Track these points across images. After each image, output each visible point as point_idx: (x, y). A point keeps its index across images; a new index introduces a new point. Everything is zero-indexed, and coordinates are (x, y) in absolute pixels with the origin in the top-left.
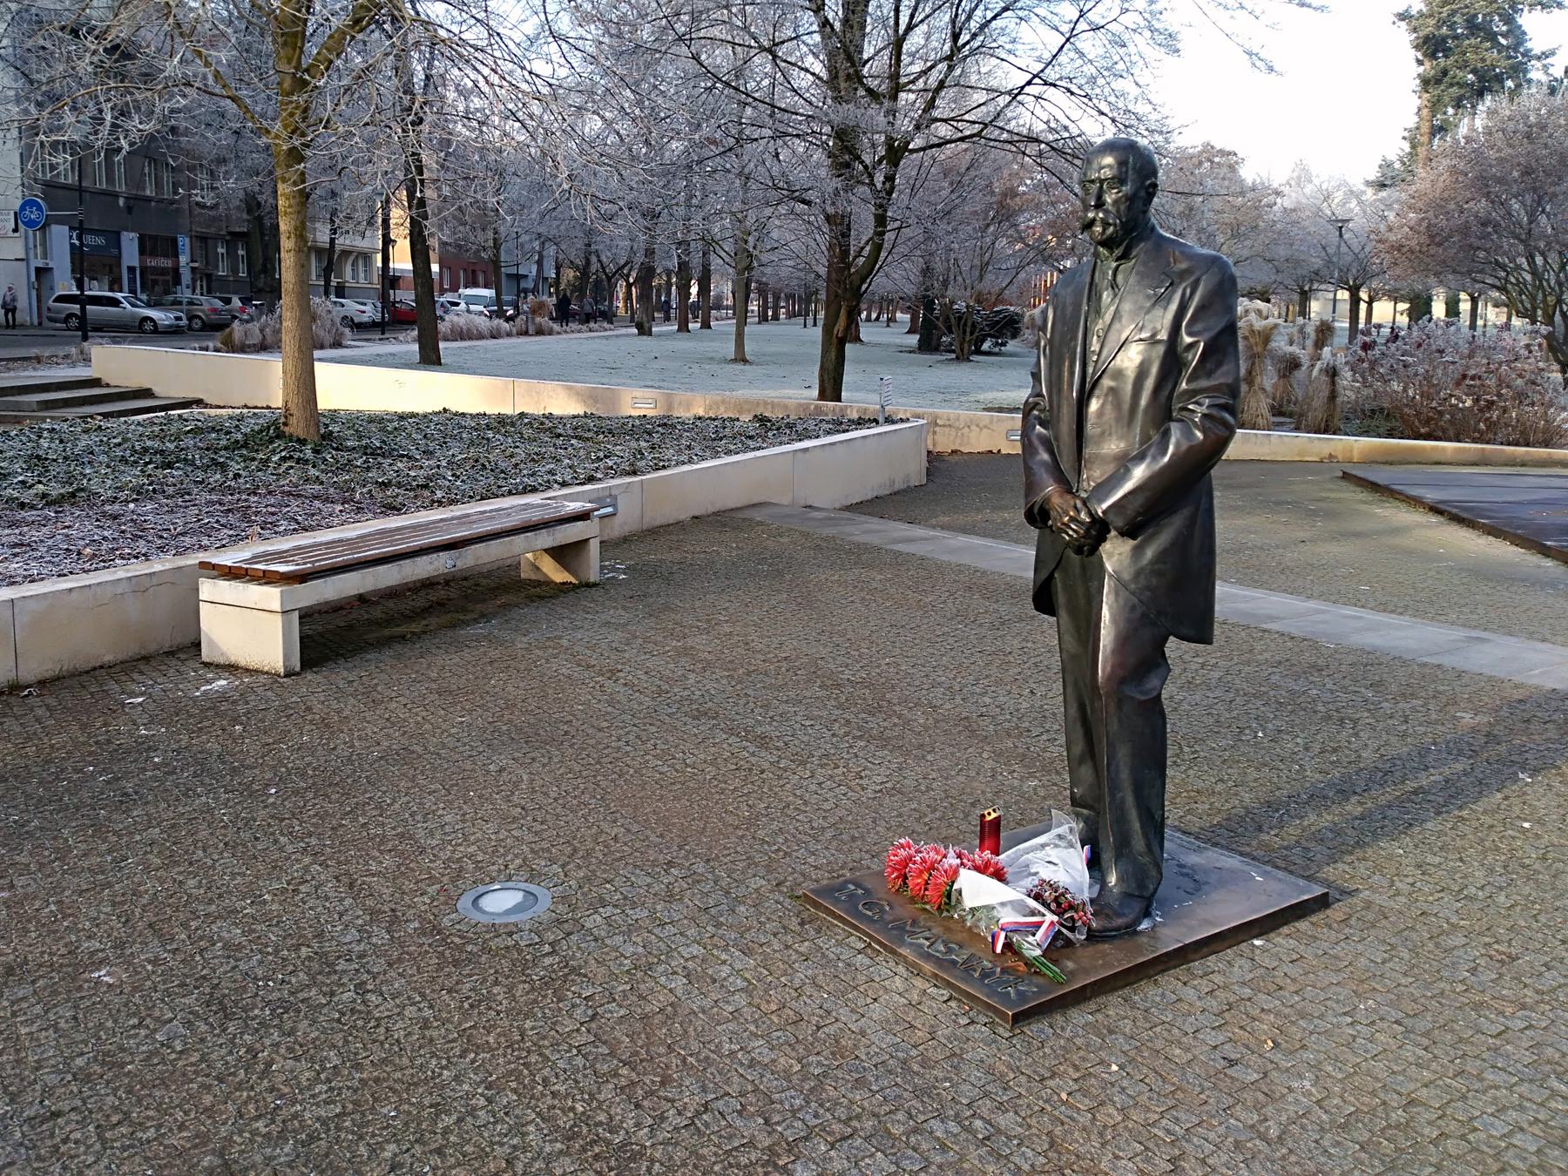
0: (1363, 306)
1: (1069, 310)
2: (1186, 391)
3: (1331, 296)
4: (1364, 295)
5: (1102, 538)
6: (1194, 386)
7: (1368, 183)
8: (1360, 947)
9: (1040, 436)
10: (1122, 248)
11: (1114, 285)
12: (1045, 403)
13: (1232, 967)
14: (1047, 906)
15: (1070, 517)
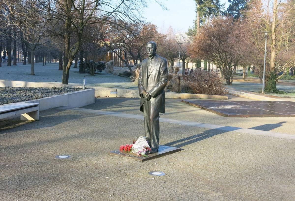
0: (186, 64)
1: (145, 65)
3: (178, 61)
4: (186, 61)
5: (150, 98)
6: (162, 76)
7: (186, 33)
10: (152, 57)
11: (151, 62)
12: (141, 79)
15: (146, 96)
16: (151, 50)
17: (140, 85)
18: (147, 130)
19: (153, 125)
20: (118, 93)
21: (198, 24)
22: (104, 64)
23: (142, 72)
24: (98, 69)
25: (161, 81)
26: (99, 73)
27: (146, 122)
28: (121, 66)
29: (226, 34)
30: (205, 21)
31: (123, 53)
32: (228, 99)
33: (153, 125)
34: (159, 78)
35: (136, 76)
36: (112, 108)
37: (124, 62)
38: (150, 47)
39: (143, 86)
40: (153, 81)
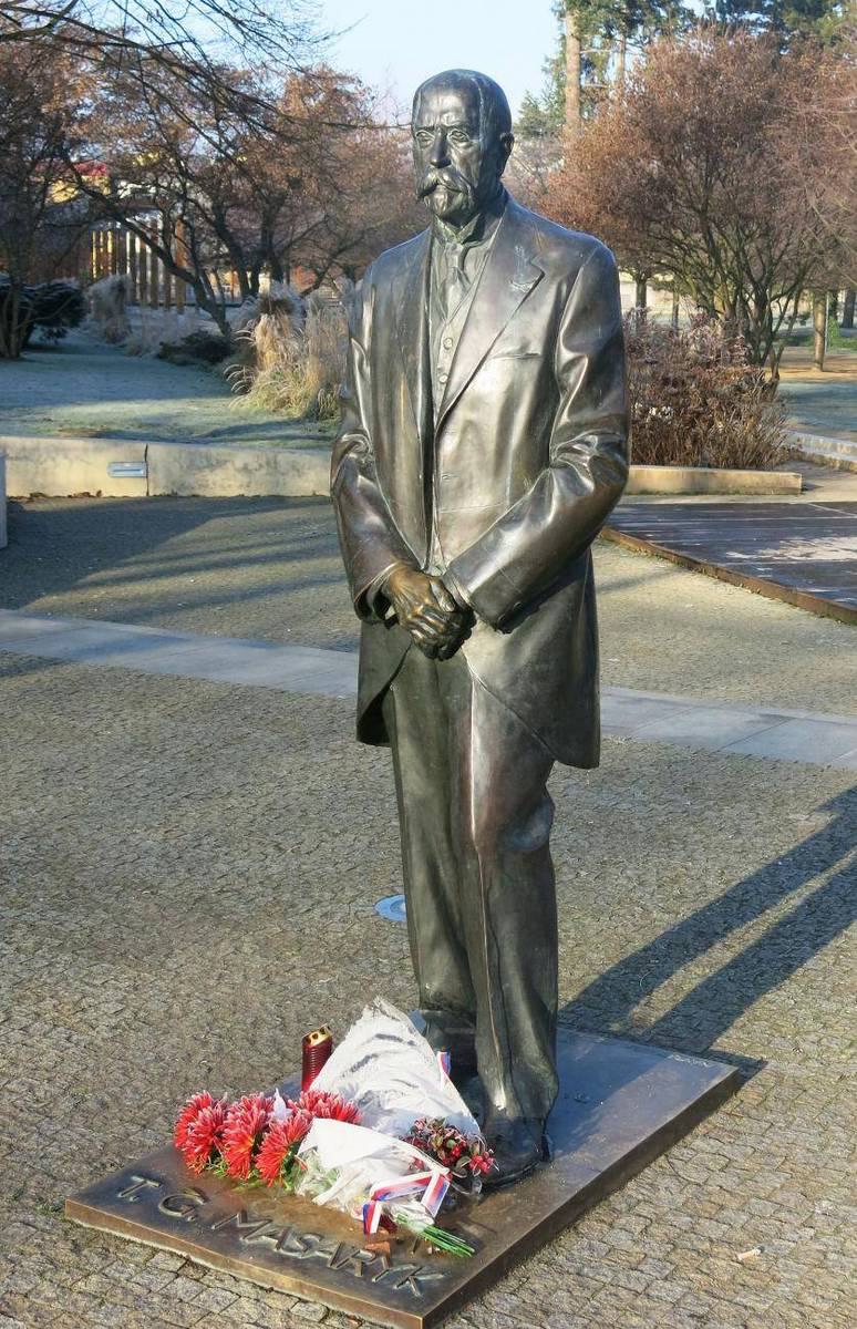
1: (400, 308)
2: (567, 427)
5: (464, 634)
6: (576, 418)
8: (790, 1135)
9: (363, 490)
11: (461, 275)
12: (367, 443)
13: (657, 1189)
14: (435, 1157)
16: (457, 152)
17: (349, 496)
18: (428, 928)
19: (496, 893)
20: (155, 470)
21: (572, 77)
22: (78, 292)
23: (367, 370)
24: (40, 323)
25: (564, 467)
26: (51, 342)
27: (415, 848)
28: (168, 305)
29: (753, 119)
30: (605, 61)
31: (179, 230)
32: (805, 489)
33: (496, 893)
34: (541, 428)
35: (255, 358)
36: (118, 581)
37: (187, 280)
38: (451, 119)
39: (384, 516)
40: (491, 467)
